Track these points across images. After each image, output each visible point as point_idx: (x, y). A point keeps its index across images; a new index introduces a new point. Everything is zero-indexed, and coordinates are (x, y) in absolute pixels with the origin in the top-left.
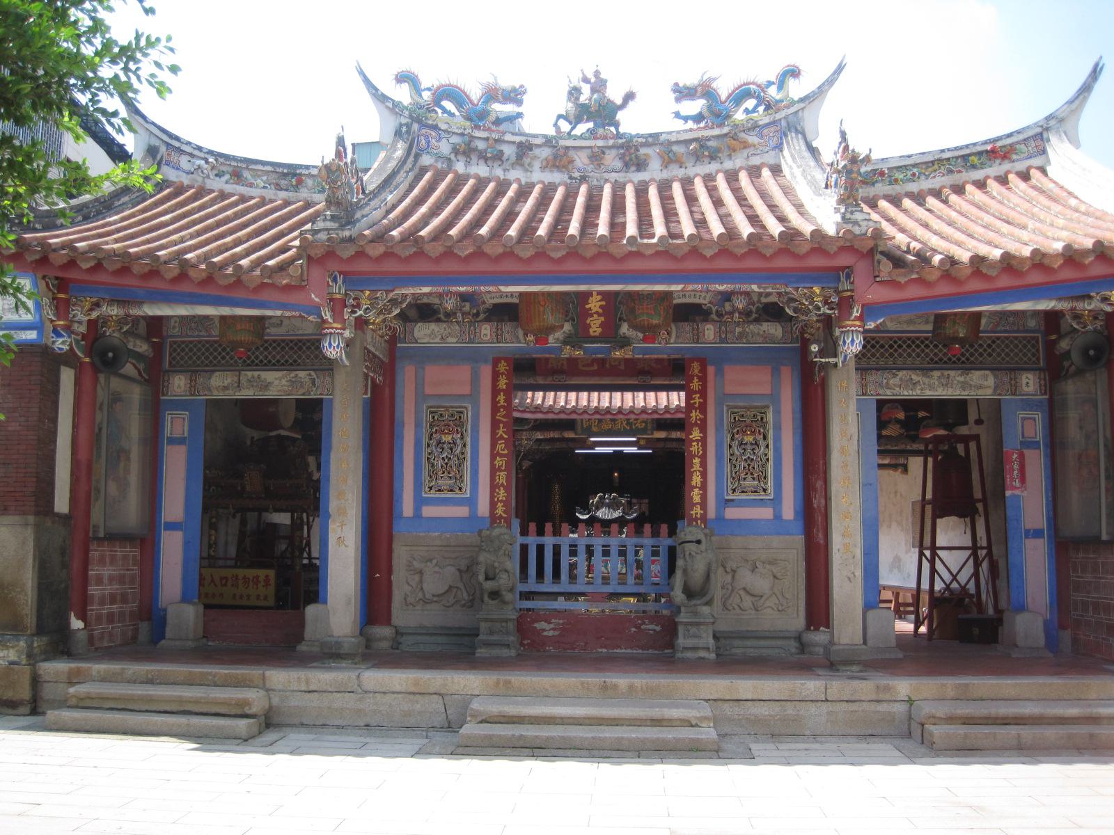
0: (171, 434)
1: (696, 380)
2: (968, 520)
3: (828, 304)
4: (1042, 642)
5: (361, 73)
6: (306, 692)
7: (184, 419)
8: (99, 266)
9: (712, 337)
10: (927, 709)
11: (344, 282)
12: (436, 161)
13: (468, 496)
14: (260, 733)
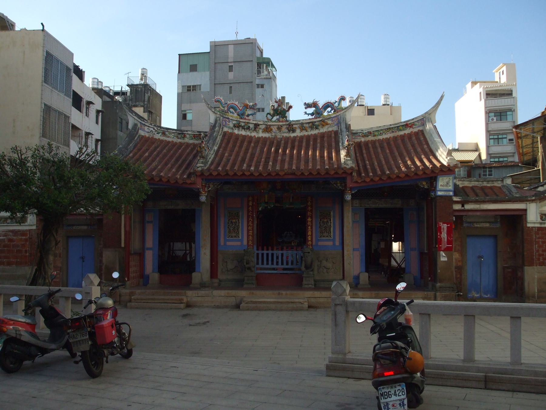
1: (309, 202)
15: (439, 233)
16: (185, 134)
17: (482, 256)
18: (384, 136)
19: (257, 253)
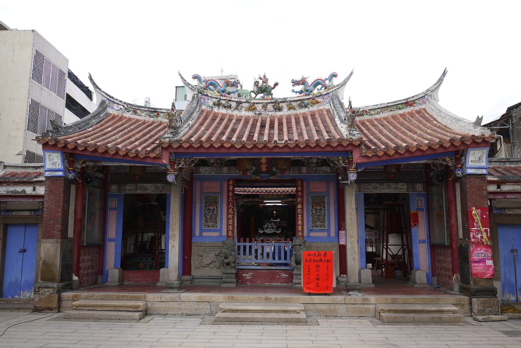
0: (111, 206)
1: (299, 187)
2: (400, 235)
3: (344, 163)
4: (425, 281)
5: (180, 75)
6: (160, 302)
7: (116, 201)
8: (86, 149)
9: (305, 172)
10: (381, 307)
11: (175, 155)
12: (207, 108)
13: (219, 228)
14: (144, 317)
15: (471, 221)
16: (158, 112)
17: (516, 249)
18: (382, 115)
19: (238, 246)
